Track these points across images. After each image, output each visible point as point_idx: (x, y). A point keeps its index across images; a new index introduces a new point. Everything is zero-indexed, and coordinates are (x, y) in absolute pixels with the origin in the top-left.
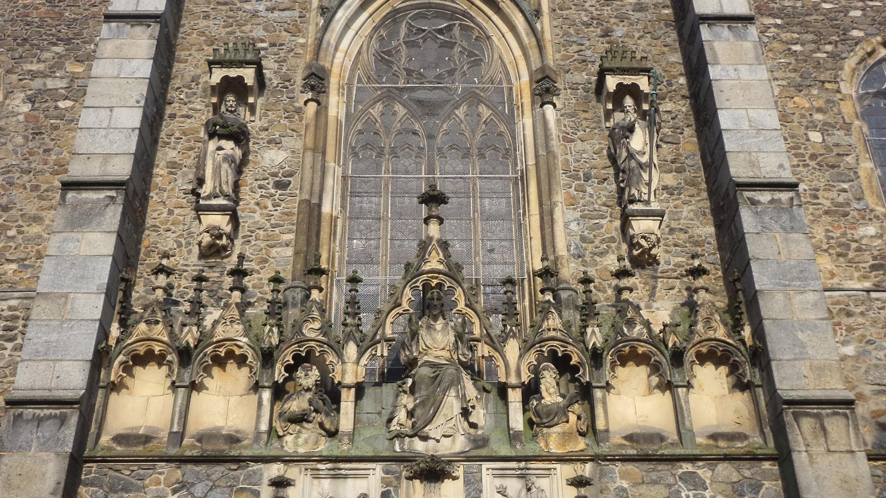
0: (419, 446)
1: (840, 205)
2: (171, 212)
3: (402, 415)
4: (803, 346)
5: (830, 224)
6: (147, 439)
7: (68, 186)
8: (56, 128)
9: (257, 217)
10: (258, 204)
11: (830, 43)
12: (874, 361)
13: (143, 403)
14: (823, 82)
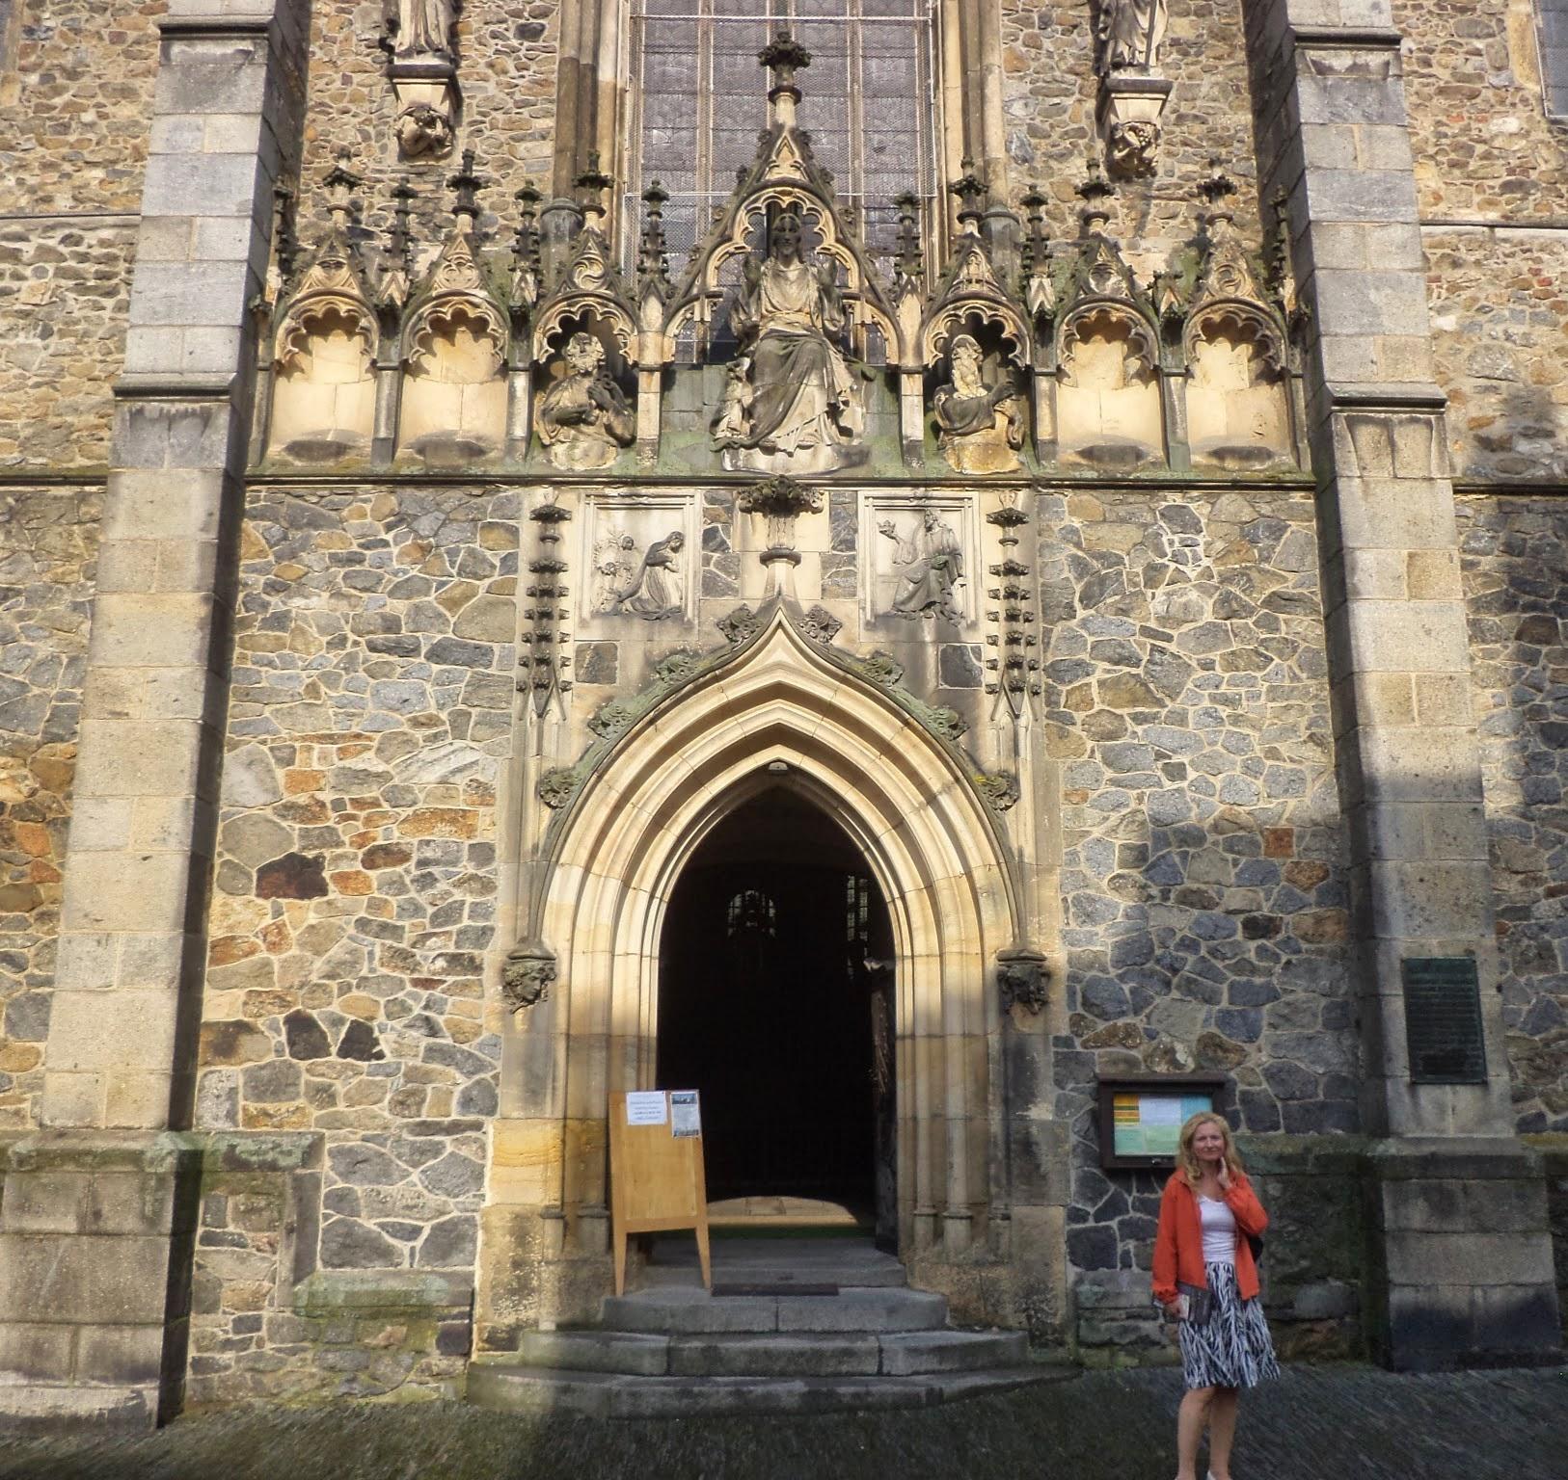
0: (761, 462)
1: (1467, 78)
2: (347, 80)
3: (734, 415)
4: (1376, 312)
5: (1447, 112)
6: (339, 449)
9: (491, 87)
10: (491, 65)
12: (1486, 341)
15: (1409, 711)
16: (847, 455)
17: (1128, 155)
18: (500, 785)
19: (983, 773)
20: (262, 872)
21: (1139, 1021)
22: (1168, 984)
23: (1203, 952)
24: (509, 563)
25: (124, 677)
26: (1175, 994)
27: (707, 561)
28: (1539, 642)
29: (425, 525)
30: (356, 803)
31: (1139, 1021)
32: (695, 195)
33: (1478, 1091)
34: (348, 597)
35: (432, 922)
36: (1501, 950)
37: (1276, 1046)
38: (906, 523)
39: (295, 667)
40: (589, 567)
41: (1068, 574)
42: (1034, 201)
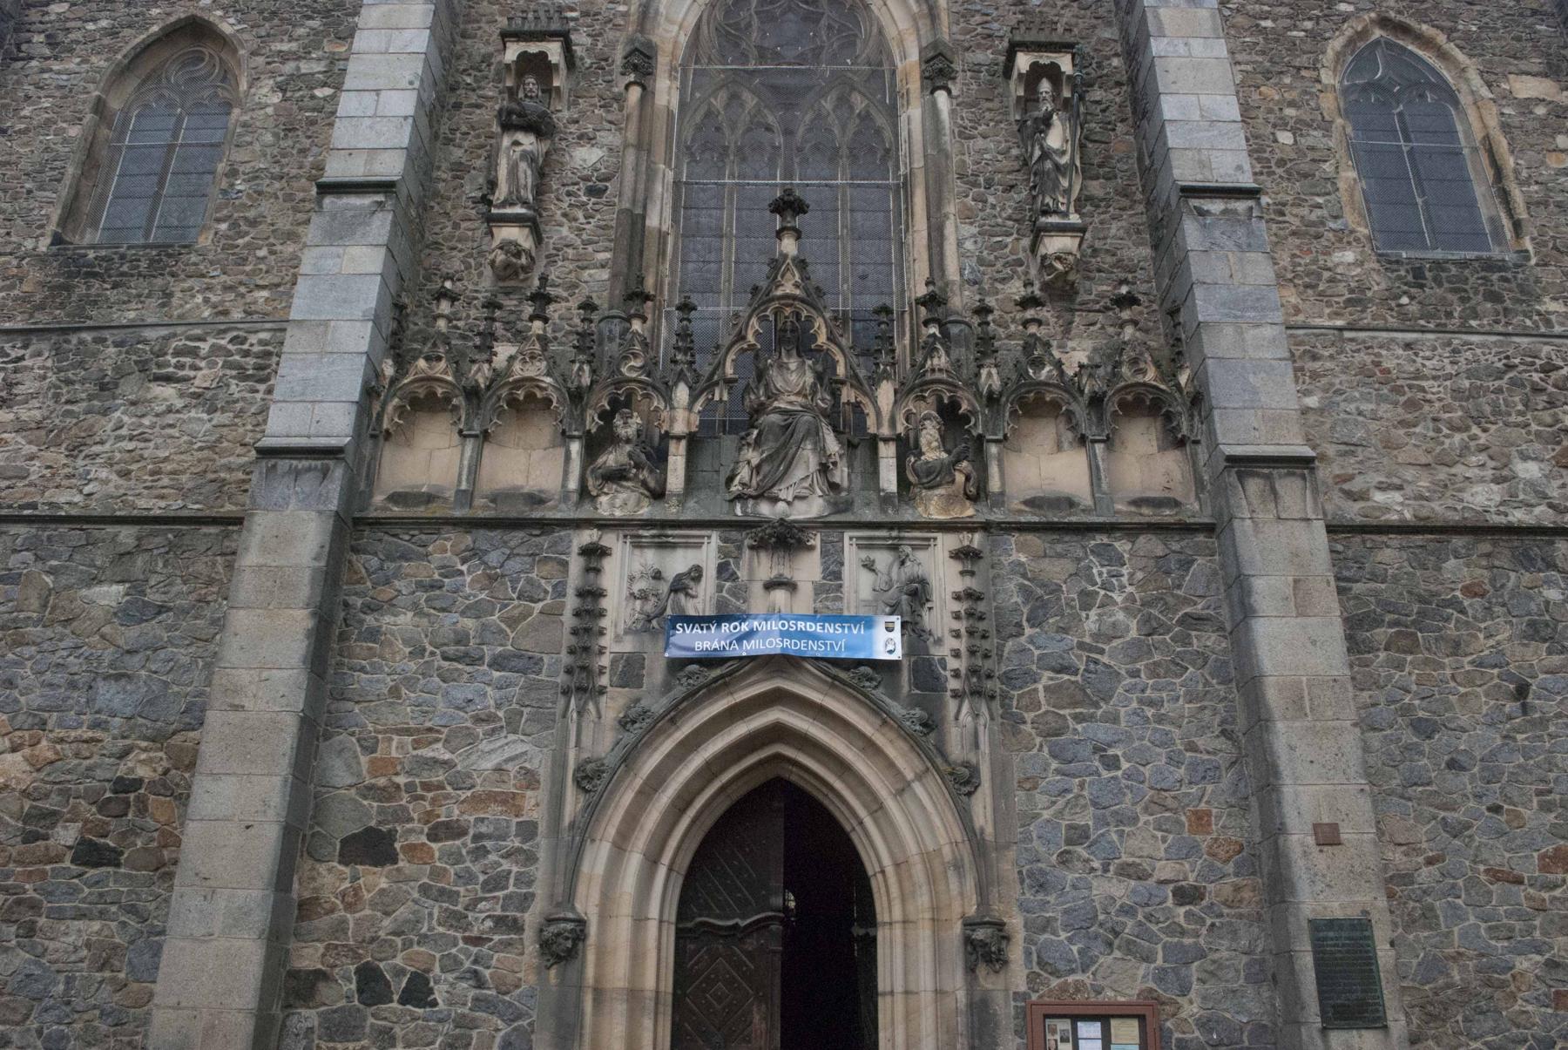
0: (765, 509)
1: (1312, 224)
2: (456, 226)
3: (744, 473)
4: (1255, 391)
5: (1298, 247)
6: (429, 498)
7: (327, 189)
8: (313, 122)
9: (565, 231)
10: (565, 215)
11: (1310, 19)
12: (1343, 415)
13: (431, 460)
14: (1299, 69)
15: (1302, 708)
16: (835, 504)
17: (1056, 278)
18: (544, 774)
19: (946, 761)
20: (344, 842)
21: (1086, 978)
22: (1110, 944)
23: (1140, 917)
24: (559, 590)
25: (244, 676)
26: (1117, 954)
27: (720, 588)
28: (1405, 652)
29: (494, 558)
30: (427, 787)
31: (1086, 978)
32: (717, 311)
33: (1379, 1035)
34: (428, 615)
35: (483, 889)
36: (1392, 912)
37: (1204, 998)
38: (883, 559)
39: (382, 672)
40: (625, 593)
41: (1017, 599)
42: (983, 310)
